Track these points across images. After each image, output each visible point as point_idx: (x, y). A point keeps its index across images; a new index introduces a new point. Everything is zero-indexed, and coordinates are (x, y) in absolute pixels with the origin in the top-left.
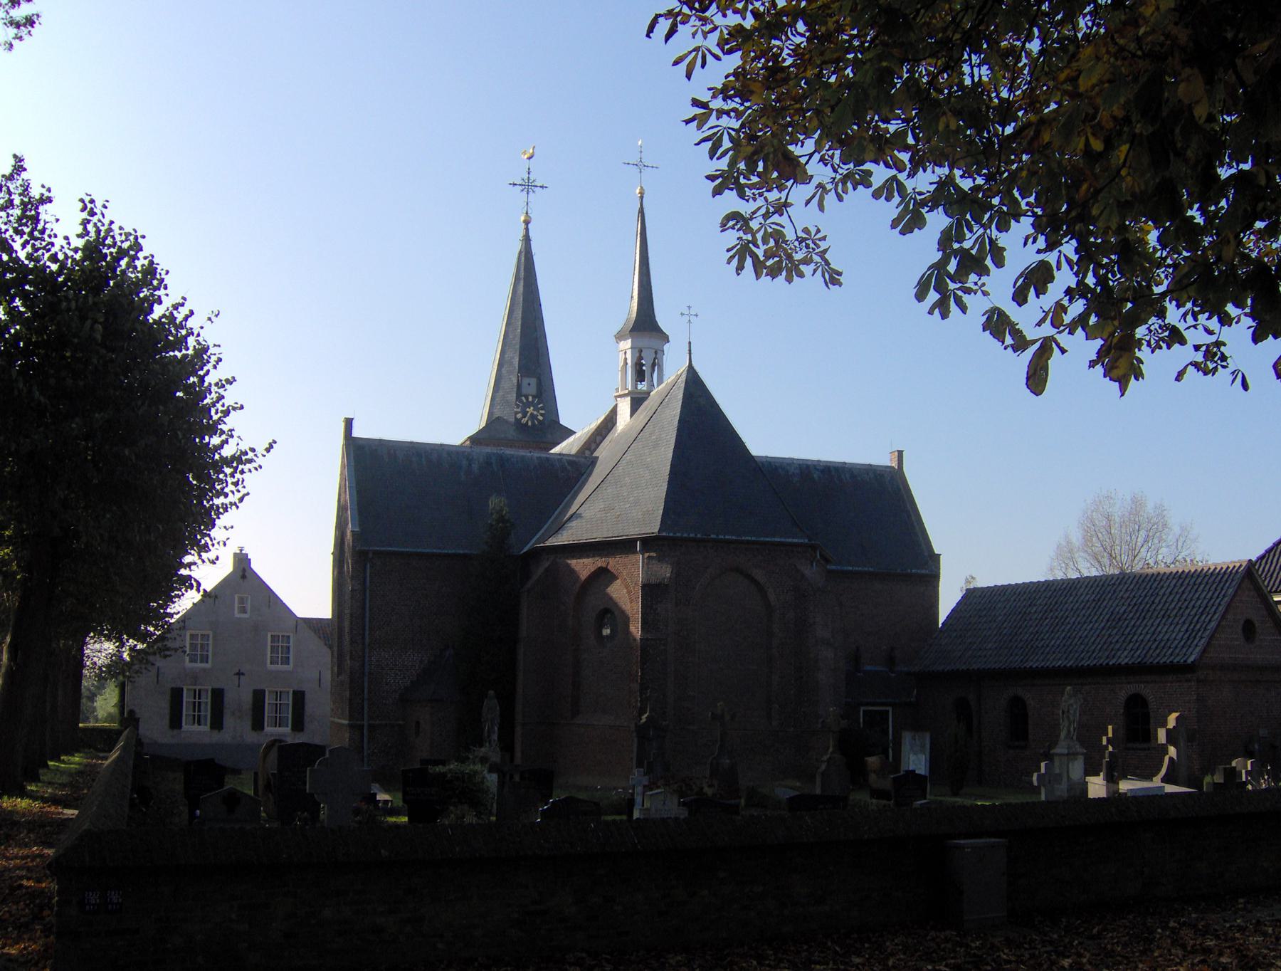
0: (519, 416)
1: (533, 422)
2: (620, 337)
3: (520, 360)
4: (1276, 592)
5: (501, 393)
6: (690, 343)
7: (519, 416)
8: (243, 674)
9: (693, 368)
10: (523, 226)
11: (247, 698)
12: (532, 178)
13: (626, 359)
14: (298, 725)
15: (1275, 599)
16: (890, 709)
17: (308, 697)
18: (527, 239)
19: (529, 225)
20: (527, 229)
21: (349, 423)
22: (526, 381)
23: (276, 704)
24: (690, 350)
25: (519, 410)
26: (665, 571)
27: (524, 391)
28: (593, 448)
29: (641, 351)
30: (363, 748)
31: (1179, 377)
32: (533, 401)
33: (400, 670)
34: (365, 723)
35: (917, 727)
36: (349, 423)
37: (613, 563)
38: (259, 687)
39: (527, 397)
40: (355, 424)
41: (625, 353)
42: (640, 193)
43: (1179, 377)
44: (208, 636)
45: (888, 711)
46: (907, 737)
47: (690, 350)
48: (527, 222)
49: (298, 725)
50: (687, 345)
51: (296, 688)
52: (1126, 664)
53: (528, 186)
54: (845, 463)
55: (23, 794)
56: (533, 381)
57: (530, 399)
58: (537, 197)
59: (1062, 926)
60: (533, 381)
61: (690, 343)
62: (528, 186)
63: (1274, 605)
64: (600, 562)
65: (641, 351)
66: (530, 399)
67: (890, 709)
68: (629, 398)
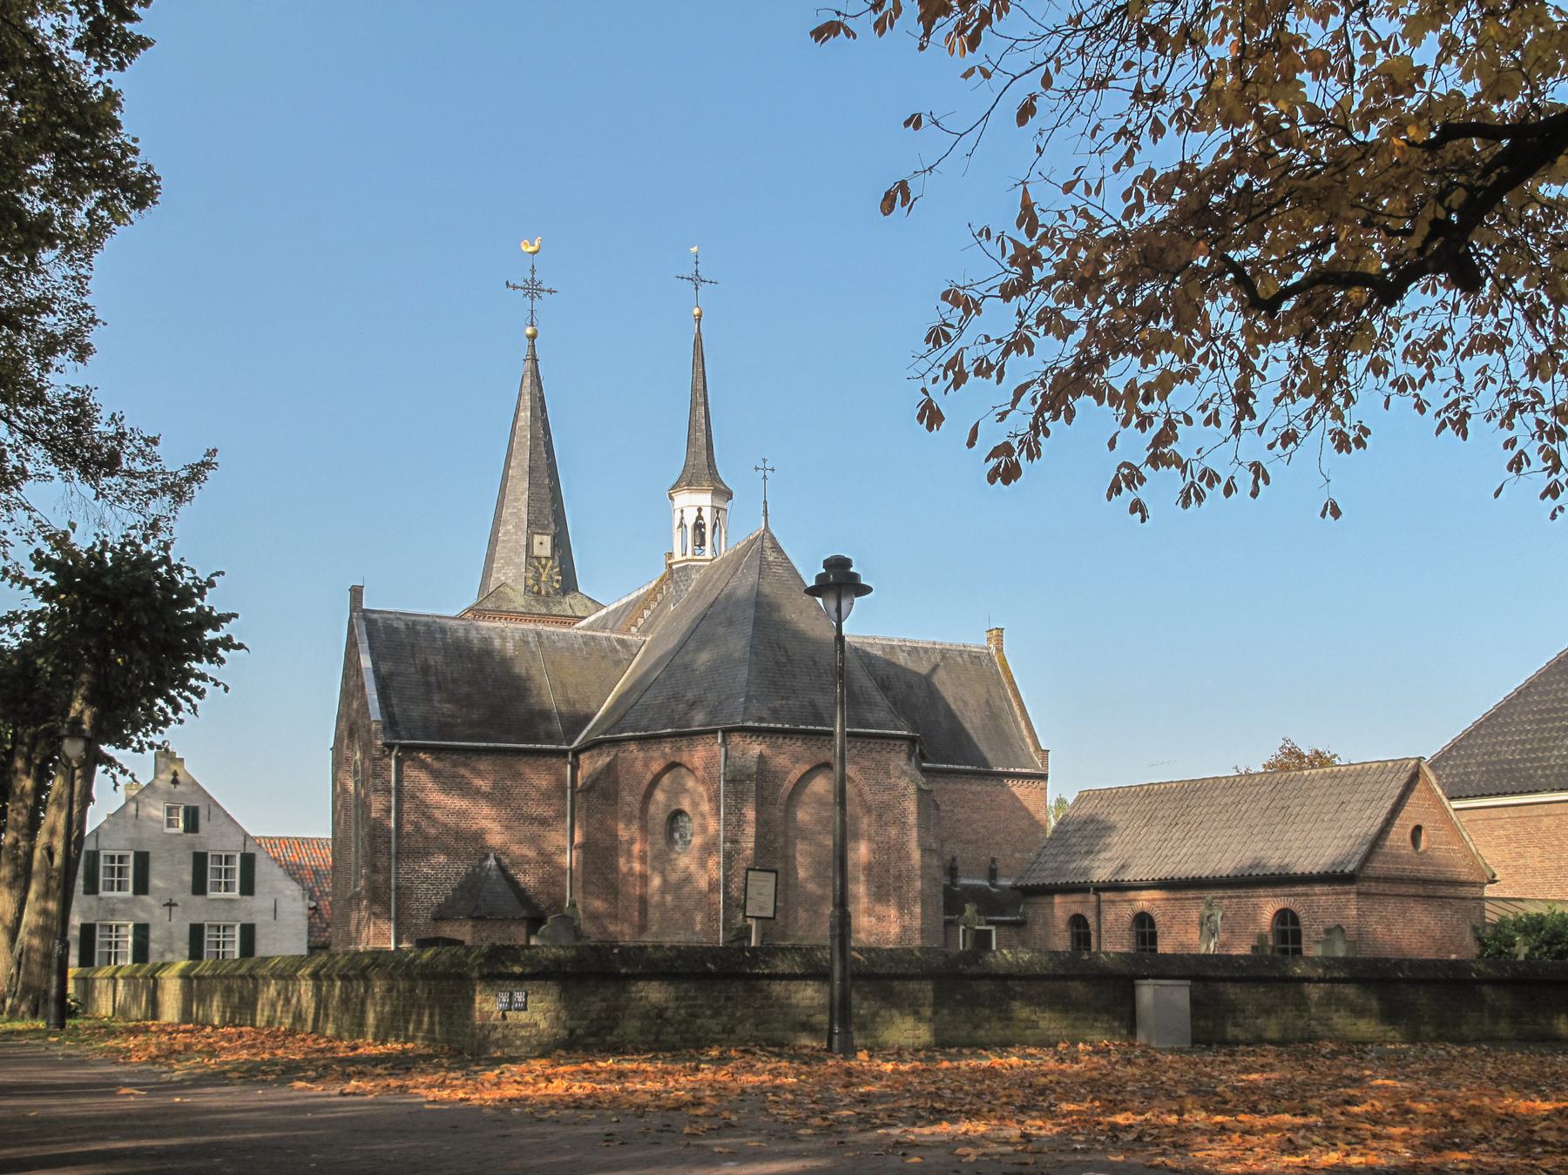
8: (176, 905)
10: (527, 342)
16: (993, 928)
21: (356, 593)
22: (537, 539)
27: (536, 552)
31: (966, 75)
36: (356, 593)
38: (248, 898)
43: (966, 75)
45: (990, 931)
51: (245, 922)
53: (533, 289)
58: (543, 304)
59: (1305, 349)
62: (533, 289)
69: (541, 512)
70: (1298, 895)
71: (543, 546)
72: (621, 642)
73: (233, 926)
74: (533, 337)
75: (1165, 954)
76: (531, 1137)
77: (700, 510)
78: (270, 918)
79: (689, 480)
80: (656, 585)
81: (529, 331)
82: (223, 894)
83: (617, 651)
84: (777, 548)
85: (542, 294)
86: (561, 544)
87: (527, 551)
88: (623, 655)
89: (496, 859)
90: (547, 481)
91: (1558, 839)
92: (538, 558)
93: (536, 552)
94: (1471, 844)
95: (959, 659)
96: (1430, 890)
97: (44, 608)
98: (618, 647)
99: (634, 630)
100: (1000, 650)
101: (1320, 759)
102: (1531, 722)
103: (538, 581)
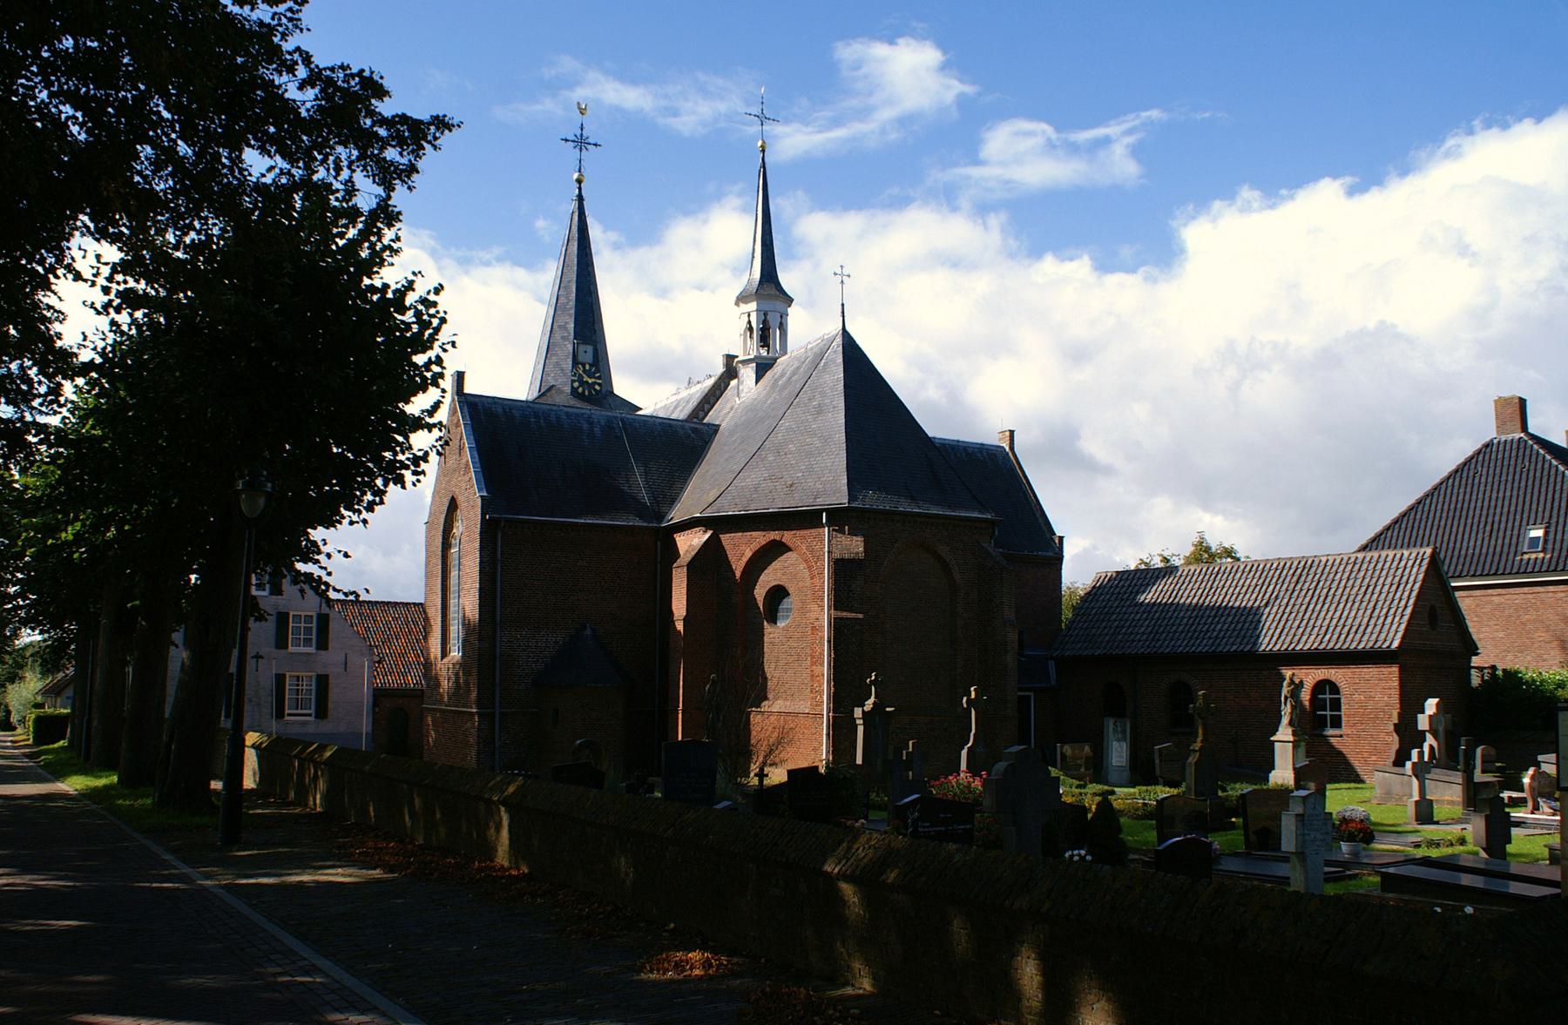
0: (576, 384)
1: (590, 392)
2: (742, 299)
3: (575, 327)
4: (1452, 577)
5: (554, 359)
6: (843, 305)
7: (576, 384)
8: (262, 657)
9: (849, 334)
11: (309, 686)
12: (585, 135)
13: (749, 322)
14: (322, 712)
15: (1453, 584)
17: (332, 681)
18: (580, 198)
19: (582, 185)
20: (580, 189)
22: (582, 348)
23: (298, 690)
24: (843, 312)
25: (576, 378)
26: (854, 546)
27: (581, 359)
28: (701, 416)
29: (765, 314)
30: (494, 739)
32: (590, 370)
33: (533, 652)
34: (1328, 713)
35: (1119, 714)
37: (788, 537)
38: (323, 652)
39: (584, 365)
40: (467, 377)
41: (749, 315)
42: (761, 146)
44: (312, 616)
45: (1030, 696)
46: (1110, 724)
47: (843, 312)
48: (579, 181)
49: (322, 712)
50: (840, 307)
52: (1130, 653)
54: (958, 441)
55: (962, 829)
56: (590, 349)
57: (587, 367)
58: (590, 154)
60: (590, 349)
61: (843, 305)
62: (581, 142)
63: (1450, 590)
64: (774, 535)
65: (765, 314)
66: (587, 367)
67: (1032, 694)
68: (754, 365)
76: (92, 673)
77: (749, 315)
78: (340, 670)
82: (302, 649)
89: (591, 628)
91: (1477, 616)
95: (979, 455)
97: (388, 256)
100: (1012, 448)
101: (1229, 553)
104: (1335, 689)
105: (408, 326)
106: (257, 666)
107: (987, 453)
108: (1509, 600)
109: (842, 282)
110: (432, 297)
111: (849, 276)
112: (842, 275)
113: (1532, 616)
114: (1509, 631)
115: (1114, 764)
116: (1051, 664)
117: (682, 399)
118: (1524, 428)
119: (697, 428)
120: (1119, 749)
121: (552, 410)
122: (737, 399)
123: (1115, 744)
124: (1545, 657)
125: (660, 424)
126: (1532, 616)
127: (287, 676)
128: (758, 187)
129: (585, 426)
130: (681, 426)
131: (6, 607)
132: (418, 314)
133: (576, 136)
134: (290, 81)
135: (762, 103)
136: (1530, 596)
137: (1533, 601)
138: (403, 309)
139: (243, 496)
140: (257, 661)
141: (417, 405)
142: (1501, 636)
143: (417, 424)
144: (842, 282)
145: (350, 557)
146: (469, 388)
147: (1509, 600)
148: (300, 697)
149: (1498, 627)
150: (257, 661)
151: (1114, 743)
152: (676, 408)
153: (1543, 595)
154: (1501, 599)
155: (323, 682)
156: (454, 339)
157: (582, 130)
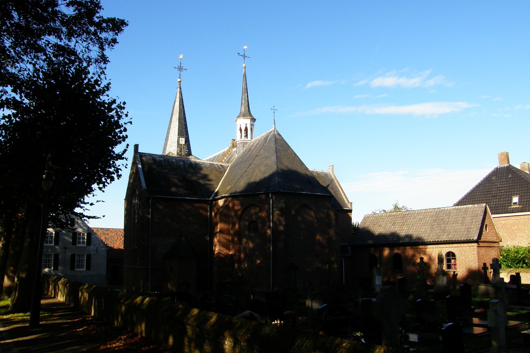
8: (67, 248)
20: (180, 84)
22: (181, 139)
27: (180, 143)
38: (89, 246)
49: (88, 268)
62: (180, 69)
67: (343, 259)
69: (182, 131)
70: (455, 247)
71: (182, 141)
72: (221, 166)
73: (84, 255)
74: (180, 82)
75: (506, 282)
77: (246, 124)
79: (244, 115)
80: (228, 149)
81: (179, 80)
83: (220, 169)
84: (279, 135)
85: (183, 70)
86: (187, 141)
87: (178, 142)
88: (222, 170)
90: (183, 122)
92: (181, 145)
93: (180, 143)
94: (497, 230)
95: (322, 174)
96: (493, 245)
98: (221, 167)
99: (223, 161)
100: (333, 172)
102: (482, 195)
103: (180, 152)
104: (453, 255)
105: (112, 117)
106: (65, 251)
107: (324, 173)
108: (507, 222)
109: (274, 112)
110: (122, 105)
111: (276, 110)
112: (274, 110)
113: (516, 227)
114: (508, 233)
115: (377, 284)
116: (349, 248)
117: (216, 156)
118: (509, 163)
119: (222, 165)
120: (378, 279)
121: (170, 158)
122: (236, 155)
123: (377, 277)
124: (521, 242)
125: (209, 163)
126: (516, 227)
127: (76, 255)
128: (243, 80)
129: (182, 163)
130: (216, 164)
131: (449, 296)
132: (117, 112)
133: (178, 66)
134: (62, 4)
135: (244, 51)
136: (515, 221)
137: (516, 222)
138: (111, 110)
139: (43, 182)
140: (65, 250)
141: (118, 149)
142: (505, 235)
143: (120, 157)
144: (274, 112)
145: (105, 216)
146: (140, 150)
147: (507, 222)
148: (80, 264)
149: (504, 232)
150: (65, 250)
151: (377, 276)
152: (214, 159)
153: (519, 220)
154: (505, 222)
155: (89, 257)
156: (131, 120)
157: (181, 64)
